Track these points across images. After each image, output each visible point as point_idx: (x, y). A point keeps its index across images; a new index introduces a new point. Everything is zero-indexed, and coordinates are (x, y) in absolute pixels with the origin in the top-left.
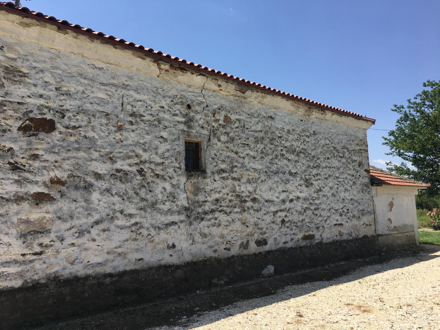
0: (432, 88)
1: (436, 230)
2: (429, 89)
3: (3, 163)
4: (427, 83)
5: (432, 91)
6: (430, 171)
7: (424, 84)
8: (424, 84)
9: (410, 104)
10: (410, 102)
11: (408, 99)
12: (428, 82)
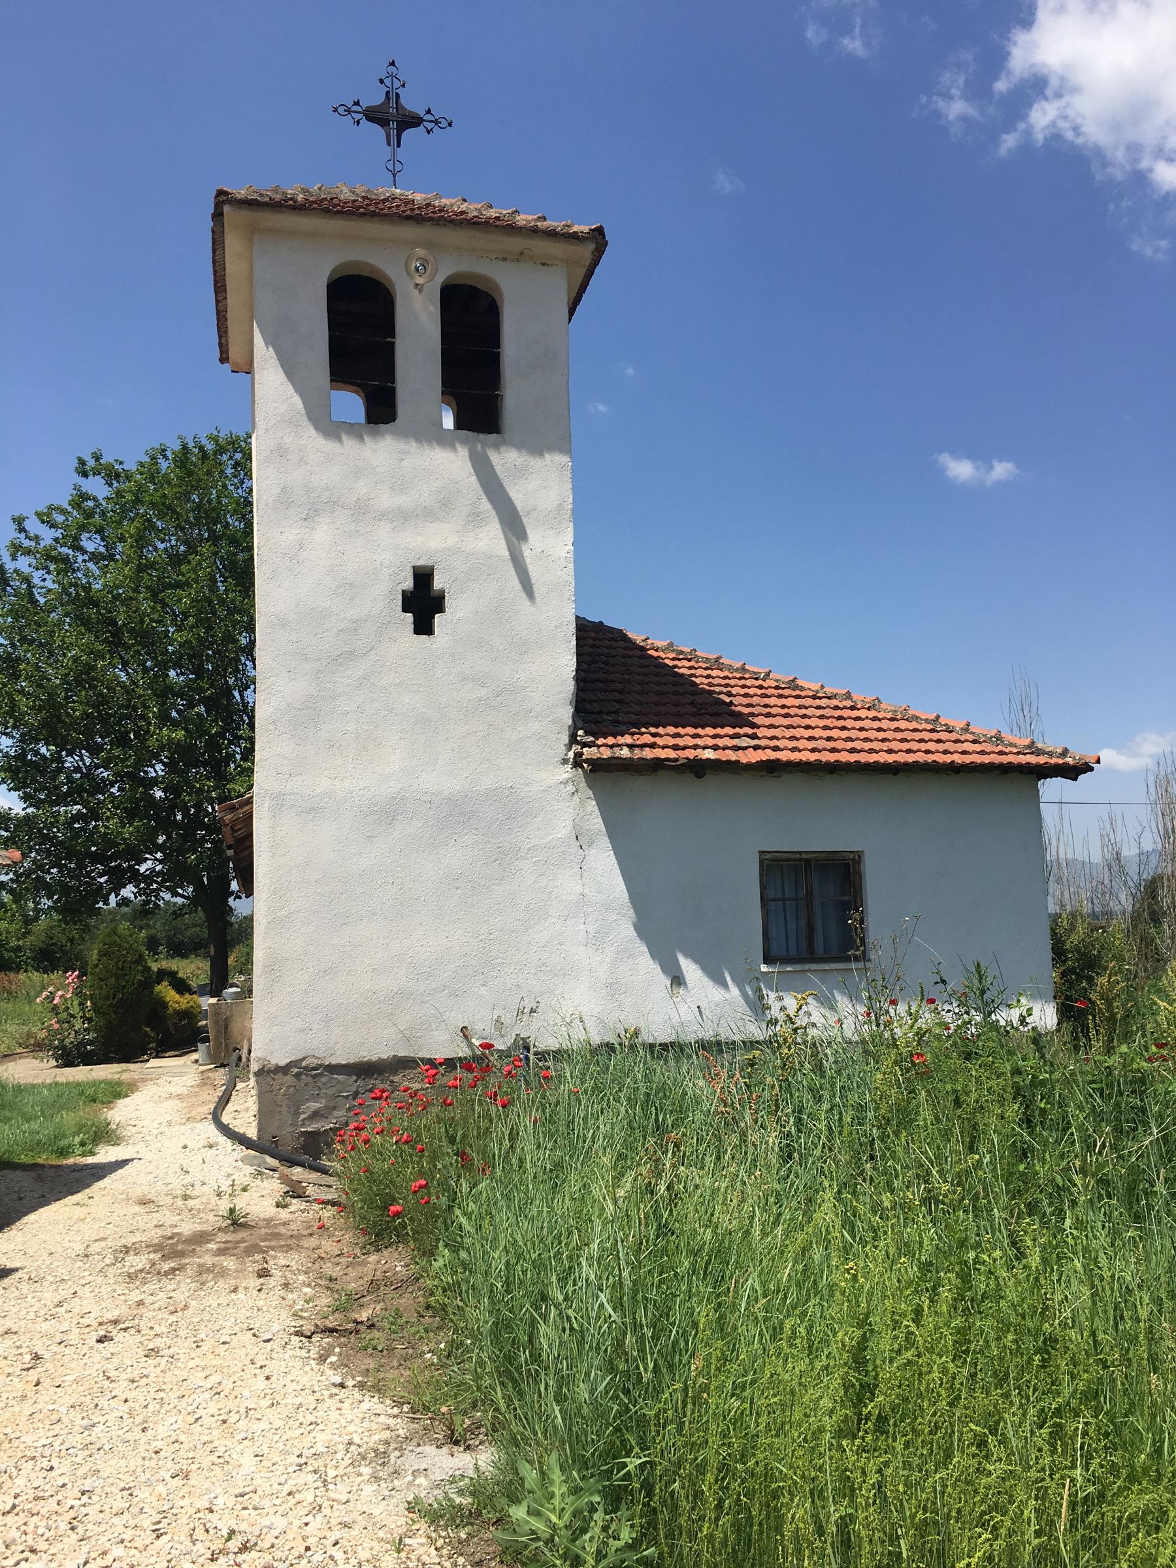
0: (110, 485)
1: (69, 1064)
2: (97, 487)
3: (774, 1432)
4: (91, 463)
5: (108, 499)
6: (77, 817)
7: (82, 462)
8: (82, 462)
9: (22, 535)
10: (22, 530)
11: (17, 514)
12: (97, 458)
